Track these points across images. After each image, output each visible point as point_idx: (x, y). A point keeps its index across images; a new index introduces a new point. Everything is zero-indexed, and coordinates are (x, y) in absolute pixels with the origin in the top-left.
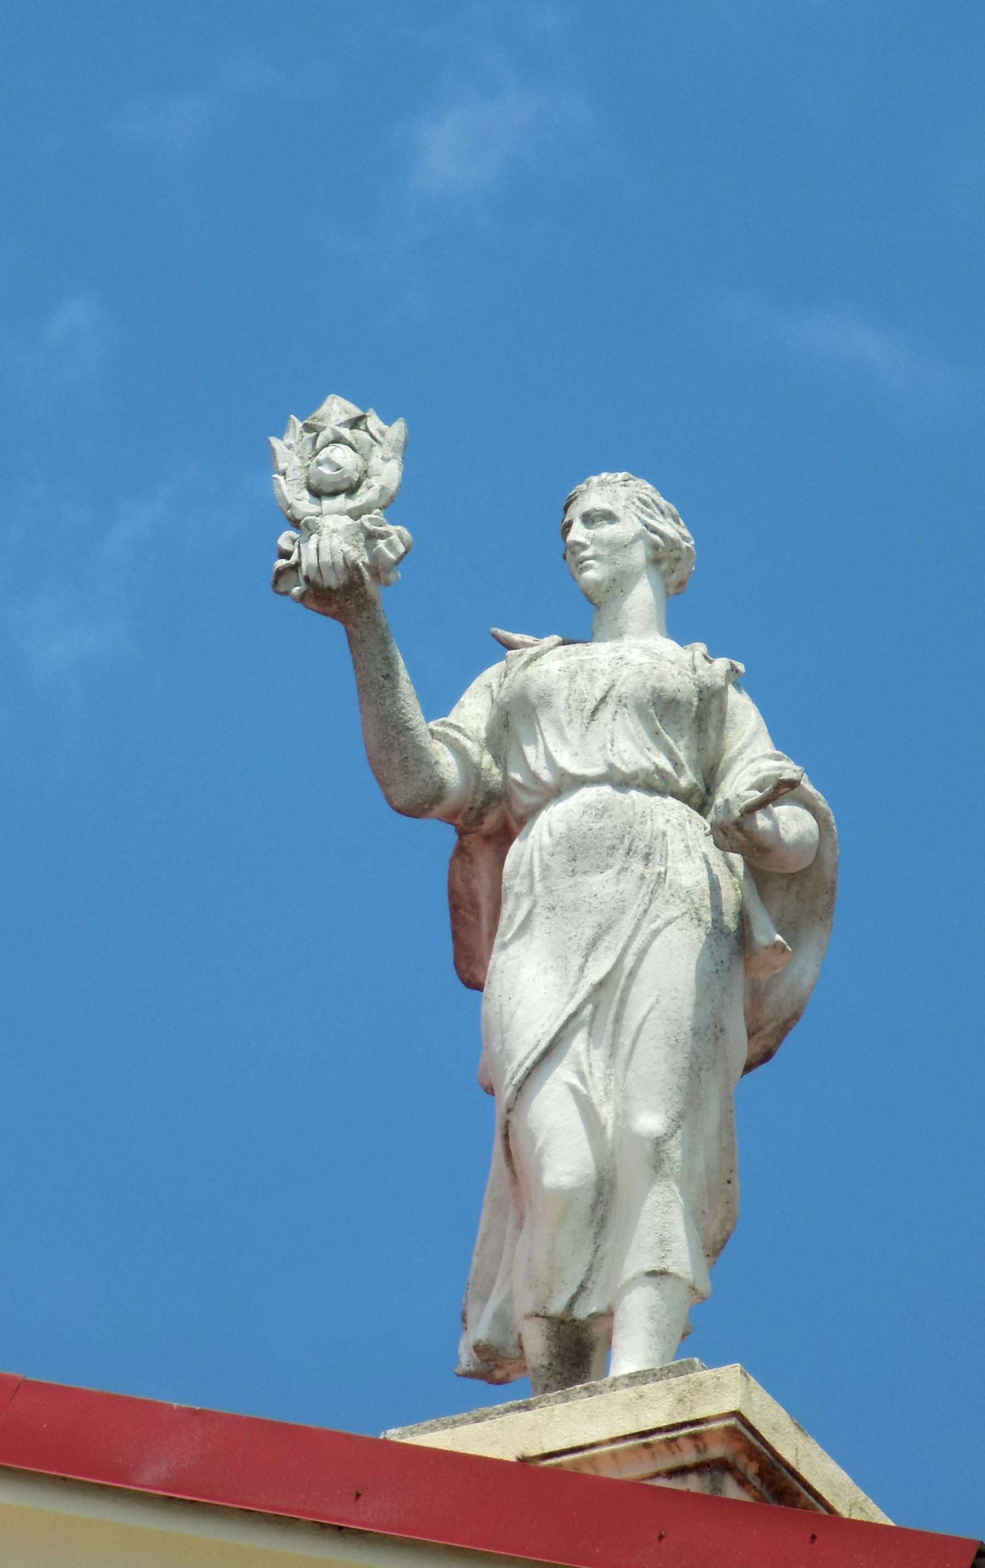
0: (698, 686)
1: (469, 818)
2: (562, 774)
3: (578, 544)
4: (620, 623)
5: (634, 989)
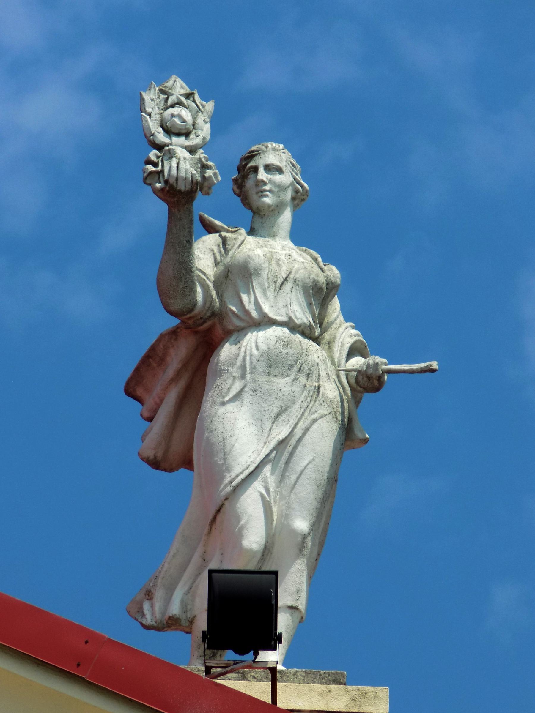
0: (326, 281)
1: (198, 322)
2: (265, 316)
3: (263, 181)
4: (275, 229)
5: (299, 448)
